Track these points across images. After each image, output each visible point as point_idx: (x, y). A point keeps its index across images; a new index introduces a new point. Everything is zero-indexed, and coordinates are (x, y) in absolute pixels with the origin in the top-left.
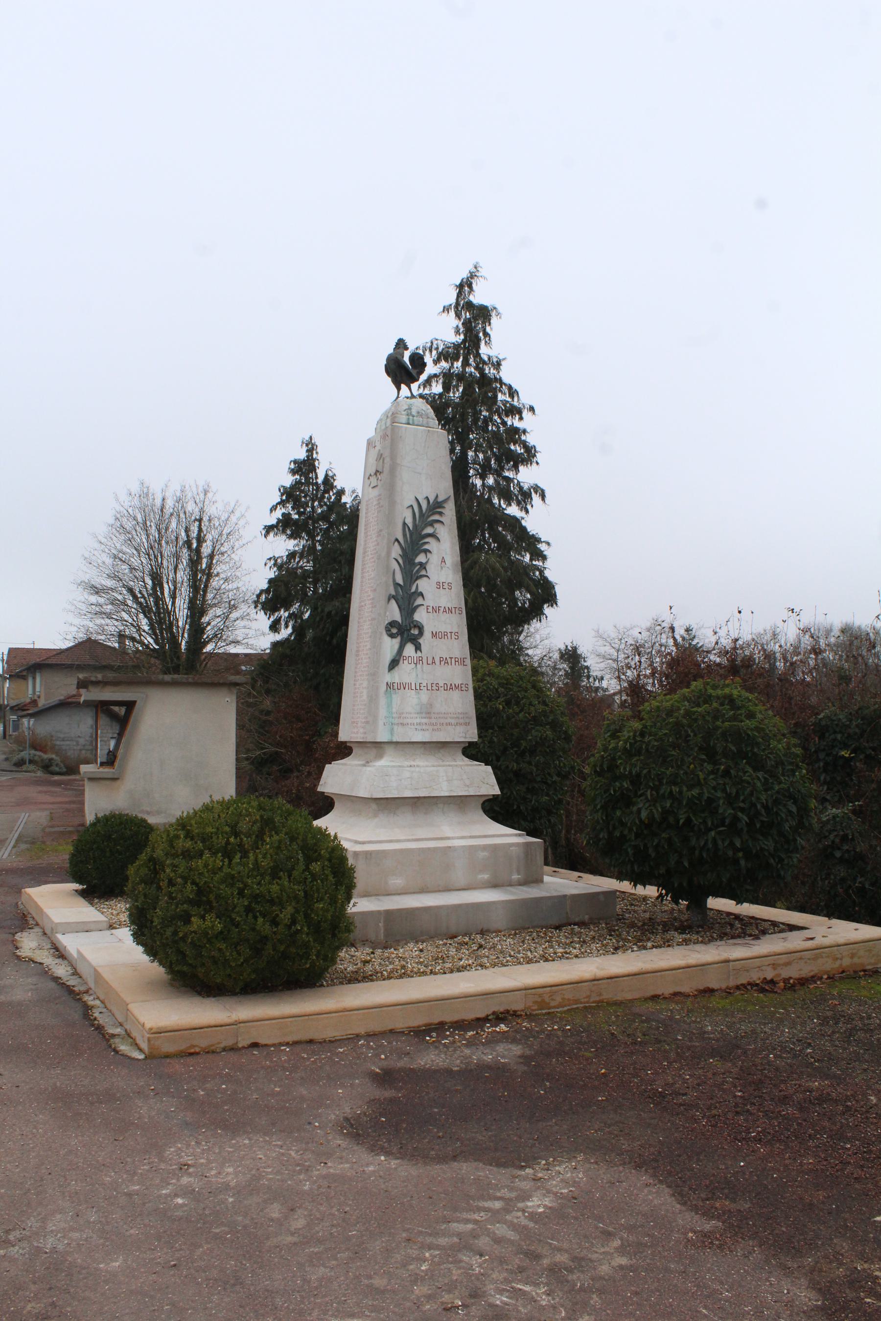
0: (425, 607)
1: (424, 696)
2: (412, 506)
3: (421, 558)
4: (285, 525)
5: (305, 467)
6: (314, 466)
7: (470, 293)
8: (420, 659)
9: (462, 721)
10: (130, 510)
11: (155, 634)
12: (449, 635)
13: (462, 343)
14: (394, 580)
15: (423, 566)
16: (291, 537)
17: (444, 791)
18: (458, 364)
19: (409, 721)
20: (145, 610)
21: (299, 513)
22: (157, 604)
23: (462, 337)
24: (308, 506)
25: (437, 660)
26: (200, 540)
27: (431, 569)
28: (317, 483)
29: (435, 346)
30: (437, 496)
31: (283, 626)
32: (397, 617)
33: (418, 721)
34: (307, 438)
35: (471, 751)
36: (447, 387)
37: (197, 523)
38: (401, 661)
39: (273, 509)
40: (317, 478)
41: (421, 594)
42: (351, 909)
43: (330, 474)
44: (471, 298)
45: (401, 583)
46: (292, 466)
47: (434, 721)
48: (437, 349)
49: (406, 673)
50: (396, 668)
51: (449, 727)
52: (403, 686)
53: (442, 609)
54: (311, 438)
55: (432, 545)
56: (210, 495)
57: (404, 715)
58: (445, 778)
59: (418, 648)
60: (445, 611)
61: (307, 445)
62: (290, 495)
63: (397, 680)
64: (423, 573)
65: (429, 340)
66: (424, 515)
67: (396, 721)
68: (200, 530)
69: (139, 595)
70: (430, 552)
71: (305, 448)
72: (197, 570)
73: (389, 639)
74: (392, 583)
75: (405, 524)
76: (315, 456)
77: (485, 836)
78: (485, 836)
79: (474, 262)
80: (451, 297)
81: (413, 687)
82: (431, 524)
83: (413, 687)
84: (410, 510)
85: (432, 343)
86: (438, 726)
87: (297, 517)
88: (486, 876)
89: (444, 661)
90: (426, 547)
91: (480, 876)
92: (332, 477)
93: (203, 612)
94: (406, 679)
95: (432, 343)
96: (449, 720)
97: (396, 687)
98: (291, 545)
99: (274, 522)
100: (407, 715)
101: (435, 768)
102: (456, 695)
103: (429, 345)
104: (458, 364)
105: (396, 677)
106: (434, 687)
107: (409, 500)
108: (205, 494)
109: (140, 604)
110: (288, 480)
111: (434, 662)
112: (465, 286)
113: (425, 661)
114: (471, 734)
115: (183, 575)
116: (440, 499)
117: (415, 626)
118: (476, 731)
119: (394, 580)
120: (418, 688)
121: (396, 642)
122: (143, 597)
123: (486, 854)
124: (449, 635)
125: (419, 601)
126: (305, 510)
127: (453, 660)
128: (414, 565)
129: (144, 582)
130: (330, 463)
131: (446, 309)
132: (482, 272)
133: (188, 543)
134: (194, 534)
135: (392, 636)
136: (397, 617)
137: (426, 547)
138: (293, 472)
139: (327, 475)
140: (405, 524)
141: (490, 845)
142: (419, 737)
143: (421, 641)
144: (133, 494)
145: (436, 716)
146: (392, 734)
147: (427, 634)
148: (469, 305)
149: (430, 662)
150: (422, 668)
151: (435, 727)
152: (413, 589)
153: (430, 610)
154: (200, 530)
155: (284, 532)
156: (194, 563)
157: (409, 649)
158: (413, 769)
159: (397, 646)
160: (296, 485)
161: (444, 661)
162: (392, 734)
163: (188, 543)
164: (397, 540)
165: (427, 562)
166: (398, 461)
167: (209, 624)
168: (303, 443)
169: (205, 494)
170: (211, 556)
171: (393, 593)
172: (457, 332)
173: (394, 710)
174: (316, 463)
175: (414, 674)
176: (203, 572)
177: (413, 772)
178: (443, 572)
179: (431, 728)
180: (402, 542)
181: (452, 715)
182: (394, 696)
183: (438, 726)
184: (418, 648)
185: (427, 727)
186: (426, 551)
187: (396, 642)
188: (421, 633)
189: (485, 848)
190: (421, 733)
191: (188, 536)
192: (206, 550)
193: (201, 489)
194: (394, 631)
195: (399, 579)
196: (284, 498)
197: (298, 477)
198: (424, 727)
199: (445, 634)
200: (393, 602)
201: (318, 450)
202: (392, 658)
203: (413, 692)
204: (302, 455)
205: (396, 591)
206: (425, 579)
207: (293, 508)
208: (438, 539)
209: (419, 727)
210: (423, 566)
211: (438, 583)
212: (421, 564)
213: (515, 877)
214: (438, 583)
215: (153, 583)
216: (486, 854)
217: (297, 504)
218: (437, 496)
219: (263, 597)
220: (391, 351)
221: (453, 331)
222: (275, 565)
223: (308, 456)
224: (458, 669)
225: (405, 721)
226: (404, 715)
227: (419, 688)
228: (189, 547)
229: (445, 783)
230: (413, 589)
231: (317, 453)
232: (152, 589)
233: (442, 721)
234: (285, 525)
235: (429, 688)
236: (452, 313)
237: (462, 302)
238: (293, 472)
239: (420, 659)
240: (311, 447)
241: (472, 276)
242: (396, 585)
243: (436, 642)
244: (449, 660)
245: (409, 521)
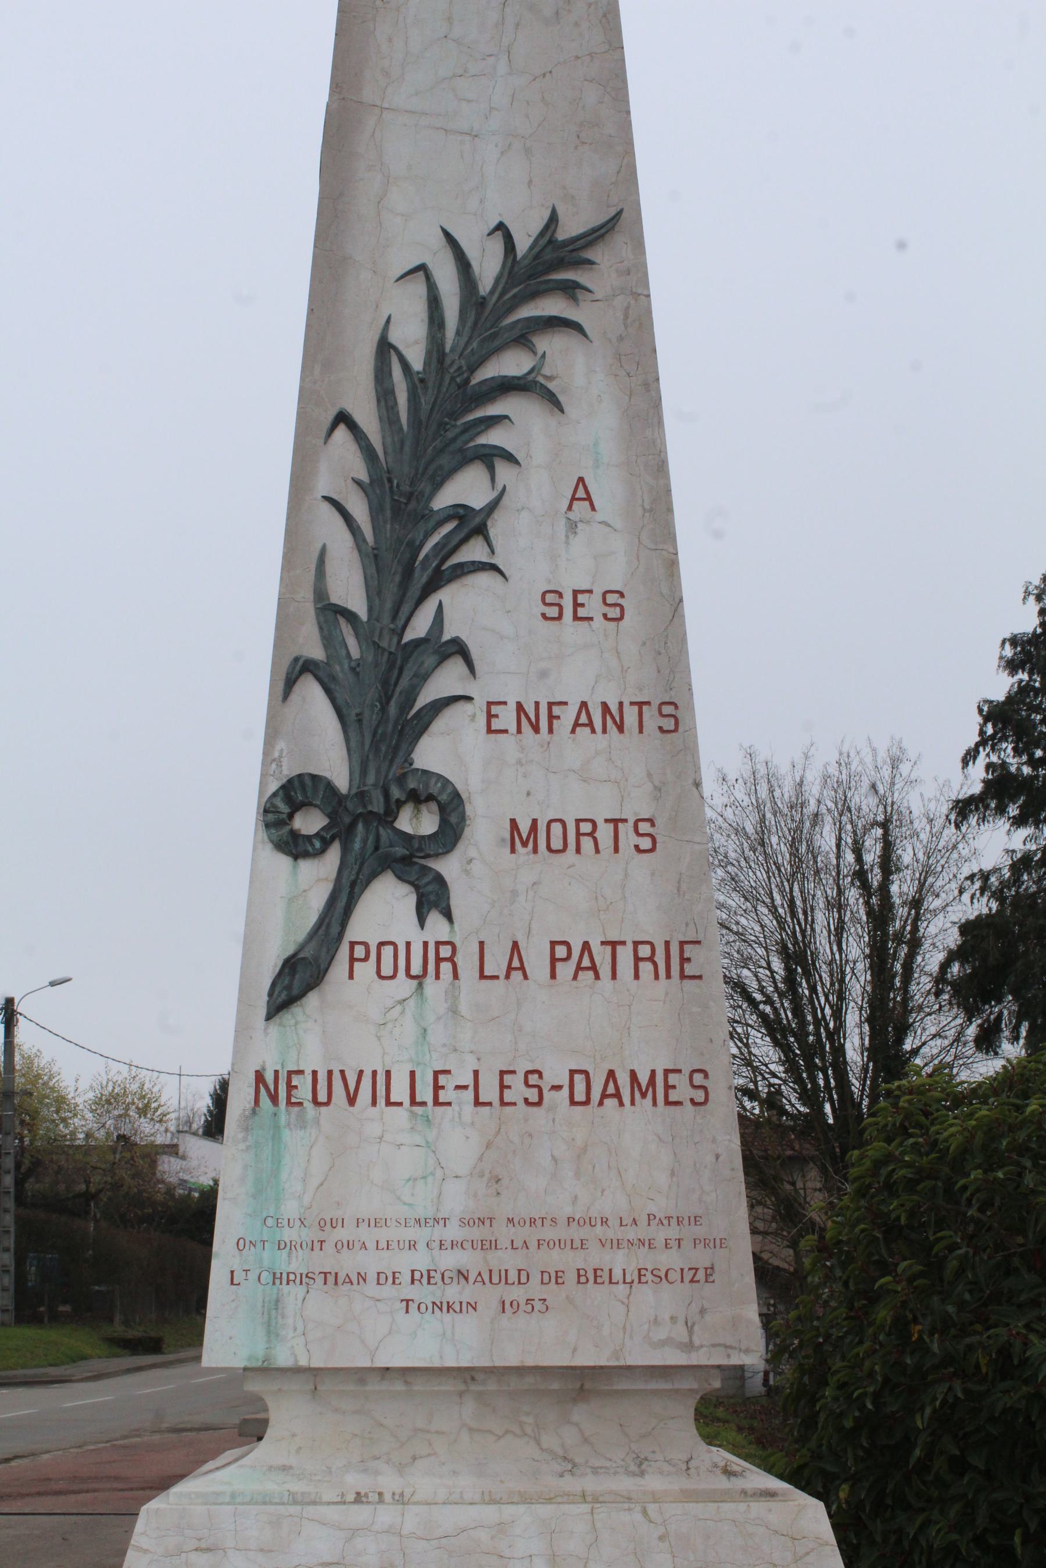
1: (460, 1133)
2: (422, 268)
3: (468, 488)
8: (442, 957)
9: (670, 1260)
10: (729, 813)
11: (799, 1080)
12: (605, 833)
14: (320, 593)
15: (473, 523)
16: (1019, 822)
19: (371, 1262)
20: (773, 1028)
22: (798, 1011)
25: (537, 960)
26: (888, 864)
27: (514, 537)
30: (553, 219)
32: (334, 763)
33: (421, 1260)
37: (879, 832)
39: (969, 757)
41: (459, 649)
45: (359, 605)
46: (1009, 652)
47: (507, 1260)
49: (360, 1019)
50: (312, 999)
51: (597, 1294)
53: (568, 716)
55: (521, 426)
56: (904, 768)
57: (342, 1234)
59: (433, 898)
60: (583, 721)
64: (474, 551)
66: (482, 302)
67: (298, 1263)
68: (888, 846)
69: (758, 997)
70: (510, 458)
72: (885, 933)
73: (284, 862)
74: (309, 609)
75: (385, 348)
81: (400, 1091)
82: (523, 337)
83: (400, 1091)
84: (418, 288)
87: (1026, 770)
90: (494, 437)
93: (903, 1029)
94: (364, 1054)
96: (595, 1258)
97: (304, 1092)
99: (977, 788)
100: (366, 1234)
101: (490, 1513)
102: (636, 1124)
105: (310, 1040)
109: (763, 1016)
110: (1000, 686)
111: (516, 964)
114: (735, 1333)
115: (856, 948)
116: (570, 228)
117: (417, 798)
118: (752, 1312)
120: (425, 1093)
122: (769, 1001)
124: (605, 833)
125: (447, 680)
127: (625, 955)
133: (861, 875)
134: (872, 856)
135: (296, 847)
137: (494, 437)
138: (1012, 666)
140: (385, 348)
142: (422, 1342)
143: (448, 867)
144: (731, 777)
145: (521, 1233)
146: (272, 1331)
147: (483, 831)
149: (496, 964)
151: (517, 1293)
152: (419, 627)
153: (507, 718)
154: (888, 846)
155: (1001, 810)
156: (880, 916)
157: (386, 909)
158: (360, 1514)
162: (272, 1331)
163: (861, 875)
164: (343, 418)
165: (493, 506)
166: (368, 94)
167: (915, 1052)
168: (1027, 593)
170: (916, 903)
171: (317, 652)
173: (290, 1209)
175: (408, 1029)
177: (355, 1532)
178: (578, 543)
179: (489, 1296)
181: (612, 1232)
182: (293, 1139)
183: (535, 1289)
184: (433, 898)
188: (451, 832)
190: (434, 1322)
191: (859, 859)
192: (901, 888)
193: (882, 754)
195: (349, 588)
196: (990, 730)
198: (453, 1293)
199: (585, 830)
200: (311, 691)
202: (291, 950)
203: (400, 1116)
205: (329, 639)
206: (483, 579)
208: (553, 401)
209: (422, 1293)
210: (473, 523)
211: (551, 597)
212: (461, 513)
214: (551, 597)
215: (787, 968)
217: (1025, 742)
218: (553, 219)
225: (348, 1263)
226: (342, 1234)
227: (429, 1096)
228: (865, 886)
230: (419, 627)
235: (489, 1091)
238: (1012, 666)
242: (331, 613)
244: (602, 956)
245: (411, 338)
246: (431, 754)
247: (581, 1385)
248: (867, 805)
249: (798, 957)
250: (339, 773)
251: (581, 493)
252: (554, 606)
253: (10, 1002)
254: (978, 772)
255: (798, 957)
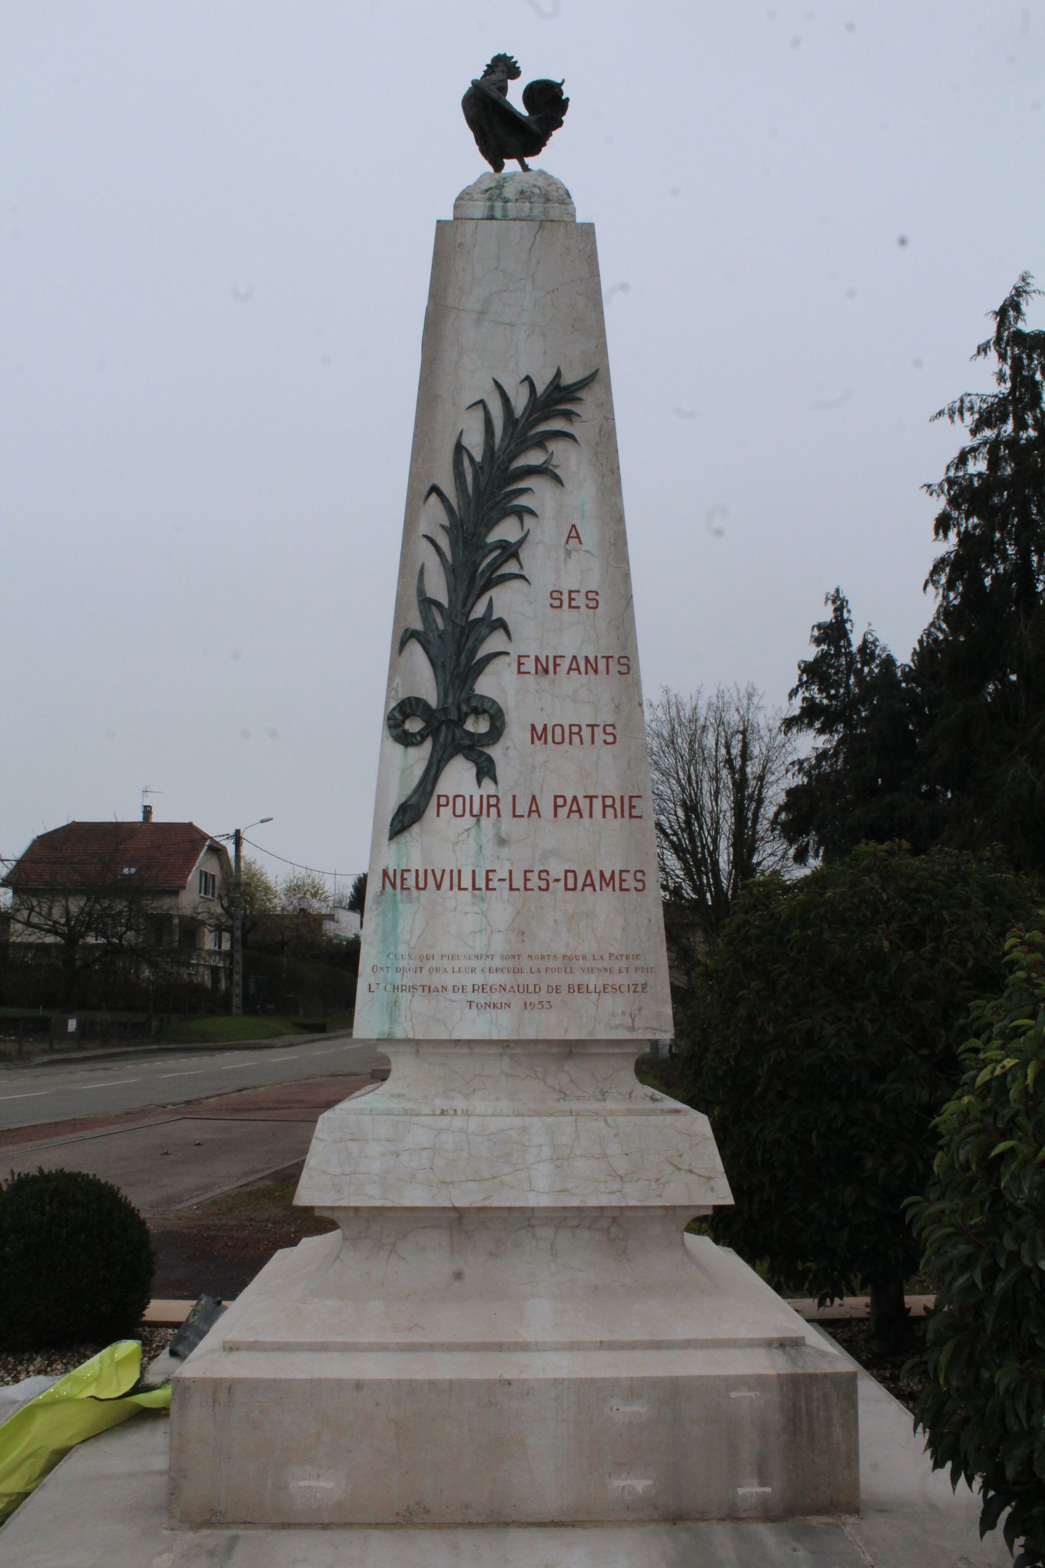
0: (512, 659)
1: (501, 908)
2: (481, 402)
3: (507, 530)
4: (810, 715)
5: (833, 632)
6: (845, 630)
7: (1016, 319)
8: (492, 804)
11: (692, 880)
12: (586, 733)
13: (1009, 394)
14: (421, 592)
15: (510, 551)
16: (821, 731)
17: (539, 1193)
18: (1009, 427)
19: (450, 980)
20: (678, 850)
21: (829, 697)
22: (692, 840)
23: (1009, 384)
24: (841, 686)
25: (546, 806)
27: (536, 559)
28: (851, 652)
29: (967, 404)
30: (558, 374)
31: (811, 853)
32: (428, 691)
33: (478, 979)
34: (832, 592)
35: (659, 1070)
36: (994, 463)
38: (431, 810)
39: (793, 693)
40: (850, 645)
41: (501, 625)
42: (867, 1299)
43: (870, 638)
44: (1021, 326)
45: (443, 599)
46: (816, 633)
48: (971, 409)
49: (445, 840)
50: (416, 828)
51: (578, 998)
52: (433, 880)
54: (837, 591)
55: (539, 494)
56: (755, 700)
57: (433, 964)
58: (546, 1152)
59: (486, 770)
61: (834, 602)
62: (813, 672)
63: (415, 862)
64: (511, 567)
65: (957, 398)
66: (516, 422)
67: (407, 980)
69: (669, 831)
70: (532, 513)
71: (831, 607)
75: (459, 449)
76: (846, 615)
77: (656, 1345)
78: (656, 1345)
79: (1020, 272)
80: (989, 330)
81: (466, 882)
82: (541, 442)
83: (466, 882)
84: (479, 413)
85: (962, 401)
86: (544, 995)
87: (825, 702)
88: (641, 1485)
89: (570, 807)
90: (522, 501)
91: (617, 1483)
92: (873, 643)
93: (752, 850)
94: (445, 860)
95: (962, 401)
97: (411, 881)
98: (822, 742)
99: (797, 712)
100: (447, 964)
101: (518, 1121)
102: (603, 903)
103: (957, 405)
104: (1009, 427)
105: (415, 851)
106: (535, 882)
107: (477, 385)
108: (749, 699)
109: (671, 842)
110: (811, 653)
111: (534, 809)
112: (1009, 310)
113: (506, 807)
115: (726, 804)
116: (569, 378)
117: (477, 712)
118: (668, 1010)
119: (421, 592)
120: (481, 883)
121: (419, 756)
122: (675, 834)
123: (638, 1409)
124: (586, 733)
125: (495, 642)
126: (837, 692)
127: (597, 804)
128: (485, 549)
129: (676, 815)
130: (870, 624)
131: (983, 349)
132: (1035, 284)
133: (729, 761)
134: (736, 751)
135: (406, 739)
136: (428, 691)
137: (522, 501)
138: (818, 641)
139: (865, 641)
140: (459, 449)
141: (655, 1383)
143: (495, 752)
146: (393, 1018)
147: (516, 733)
148: (1019, 338)
149: (522, 808)
150: (497, 825)
151: (534, 998)
152: (479, 611)
153: (529, 665)
156: (740, 785)
157: (459, 776)
158: (444, 1121)
159: (418, 771)
160: (823, 657)
161: (570, 807)
162: (393, 1018)
163: (729, 761)
164: (435, 489)
165: (521, 542)
168: (827, 599)
169: (749, 699)
170: (761, 778)
171: (419, 626)
172: (1001, 378)
174: (848, 626)
175: (471, 844)
176: (751, 798)
177: (440, 1131)
180: (449, 489)
183: (544, 995)
184: (486, 770)
185: (506, 997)
186: (521, 512)
187: (419, 756)
188: (496, 732)
189: (635, 1389)
190: (490, 1014)
191: (729, 752)
192: (753, 769)
193: (743, 692)
194: (414, 725)
195: (438, 589)
196: (805, 678)
197: (825, 647)
198: (496, 997)
199: (574, 732)
200: (415, 649)
201: (850, 606)
203: (467, 896)
204: (827, 615)
205: (426, 618)
206: (516, 584)
207: (820, 691)
208: (558, 480)
209: (480, 998)
210: (510, 551)
211: (556, 595)
213: (750, 1490)
214: (556, 595)
215: (687, 815)
216: (638, 1409)
219: (783, 816)
220: (478, 75)
221: (995, 378)
222: (799, 771)
223: (836, 617)
224: (614, 826)
225: (436, 980)
226: (433, 964)
227: (484, 884)
228: (732, 768)
229: (546, 1168)
230: (479, 611)
231: (849, 611)
232: (685, 822)
233: (556, 979)
234: (810, 715)
235: (518, 883)
236: (993, 354)
237: (1006, 334)
239: (492, 804)
240: (839, 604)
241: (1019, 292)
242: (427, 603)
243: (542, 752)
244: (584, 804)
245: (475, 443)
246: (485, 686)
247: (570, 1050)
248: (733, 718)
249: (692, 808)
250: (432, 699)
251: (574, 534)
252: (558, 599)
253: (238, 832)
254: (798, 703)
255: (692, 808)
